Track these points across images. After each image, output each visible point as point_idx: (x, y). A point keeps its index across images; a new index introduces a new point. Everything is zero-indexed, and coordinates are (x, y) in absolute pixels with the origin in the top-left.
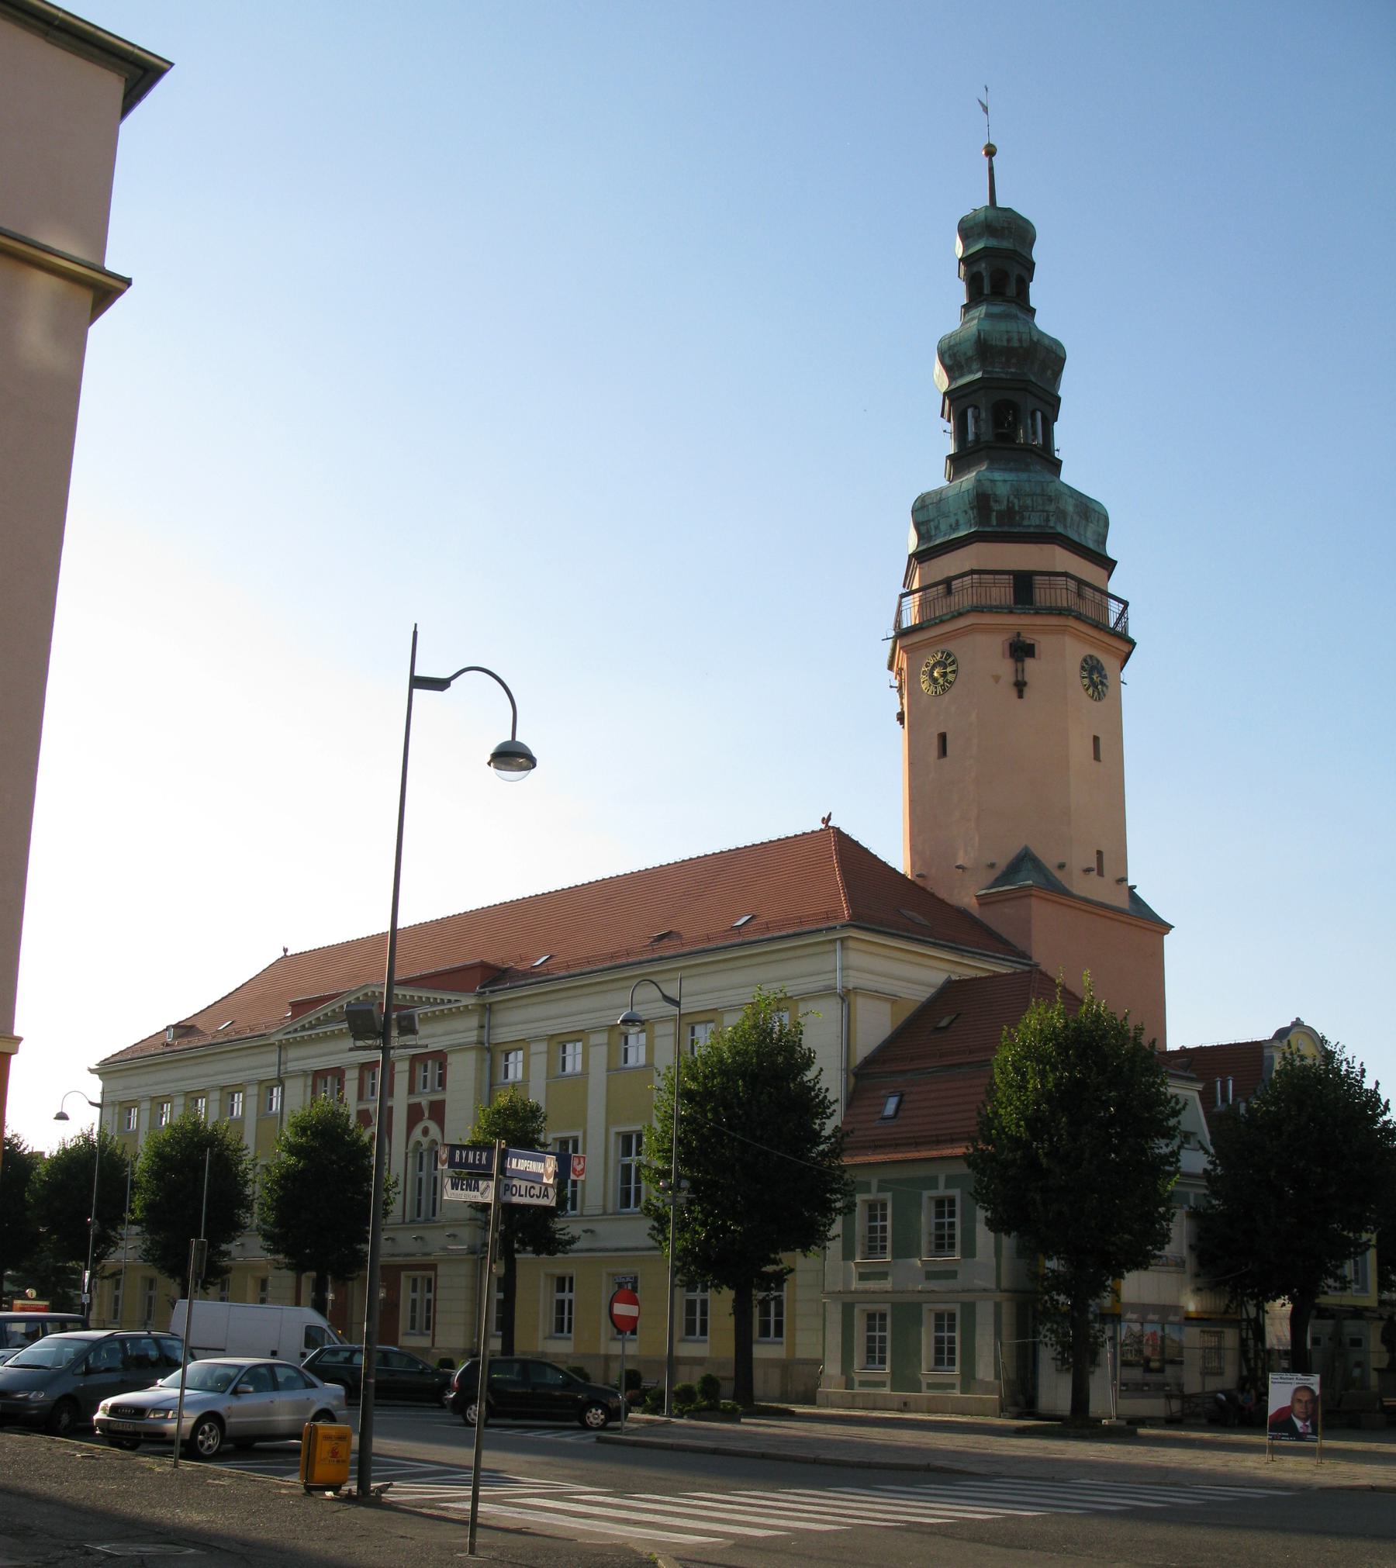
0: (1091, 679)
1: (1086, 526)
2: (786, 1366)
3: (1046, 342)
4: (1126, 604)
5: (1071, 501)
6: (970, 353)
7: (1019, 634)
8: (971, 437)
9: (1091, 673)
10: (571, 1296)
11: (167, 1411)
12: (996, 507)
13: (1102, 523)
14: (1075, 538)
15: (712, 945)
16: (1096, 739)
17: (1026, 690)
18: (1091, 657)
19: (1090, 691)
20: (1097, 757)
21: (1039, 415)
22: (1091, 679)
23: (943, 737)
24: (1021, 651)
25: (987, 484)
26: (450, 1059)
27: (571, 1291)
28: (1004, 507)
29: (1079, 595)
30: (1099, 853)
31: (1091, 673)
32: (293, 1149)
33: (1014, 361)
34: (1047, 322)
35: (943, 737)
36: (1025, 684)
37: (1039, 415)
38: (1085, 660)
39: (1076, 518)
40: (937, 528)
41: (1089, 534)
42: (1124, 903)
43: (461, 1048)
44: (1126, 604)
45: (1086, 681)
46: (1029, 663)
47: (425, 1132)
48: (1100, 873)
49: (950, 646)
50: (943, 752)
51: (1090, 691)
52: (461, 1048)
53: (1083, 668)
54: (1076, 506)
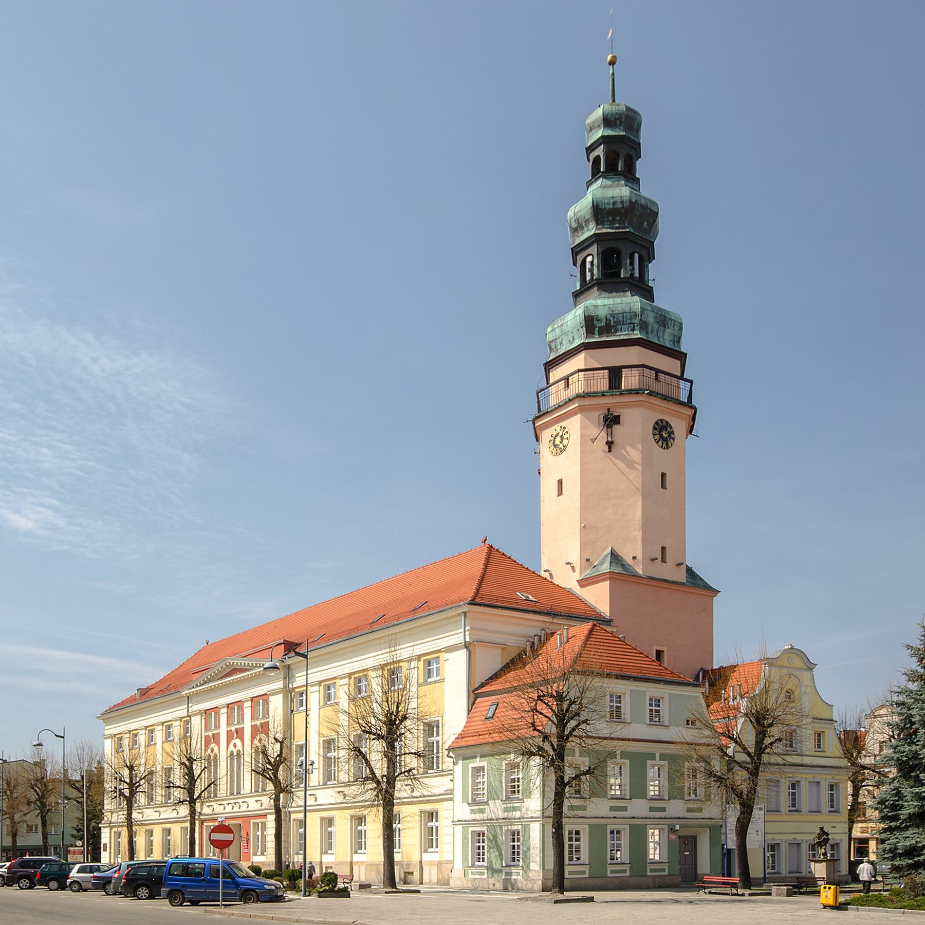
0: (661, 436)
1: (664, 333)
2: (439, 864)
3: (643, 201)
4: (691, 382)
5: (652, 315)
6: (587, 217)
7: (609, 410)
8: (588, 277)
9: (660, 431)
10: (365, 828)
11: (773, 868)
12: (598, 324)
13: (677, 328)
14: (655, 340)
15: (517, 607)
16: (663, 475)
17: (613, 446)
18: (661, 420)
19: (660, 443)
20: (663, 486)
21: (636, 255)
22: (661, 436)
23: (560, 482)
24: (611, 421)
25: (592, 308)
26: (271, 698)
27: (437, 821)
28: (603, 324)
29: (656, 379)
30: (663, 549)
31: (660, 431)
32: (913, 677)
33: (618, 218)
34: (650, 188)
35: (560, 482)
36: (612, 443)
37: (636, 255)
38: (657, 423)
39: (656, 326)
40: (561, 343)
41: (667, 336)
42: (682, 577)
43: (274, 693)
44: (691, 382)
45: (657, 437)
46: (616, 428)
47: (260, 740)
48: (664, 560)
49: (563, 424)
50: (560, 492)
51: (660, 443)
52: (274, 693)
53: (654, 428)
54: (655, 318)
